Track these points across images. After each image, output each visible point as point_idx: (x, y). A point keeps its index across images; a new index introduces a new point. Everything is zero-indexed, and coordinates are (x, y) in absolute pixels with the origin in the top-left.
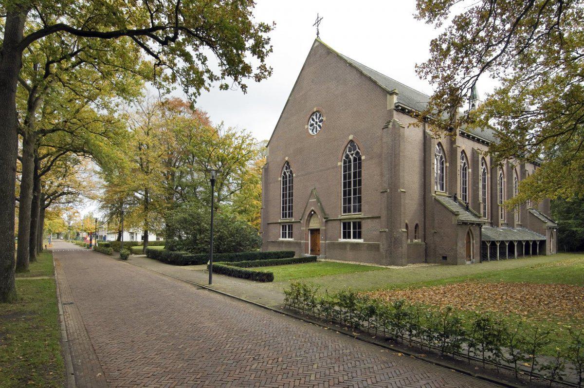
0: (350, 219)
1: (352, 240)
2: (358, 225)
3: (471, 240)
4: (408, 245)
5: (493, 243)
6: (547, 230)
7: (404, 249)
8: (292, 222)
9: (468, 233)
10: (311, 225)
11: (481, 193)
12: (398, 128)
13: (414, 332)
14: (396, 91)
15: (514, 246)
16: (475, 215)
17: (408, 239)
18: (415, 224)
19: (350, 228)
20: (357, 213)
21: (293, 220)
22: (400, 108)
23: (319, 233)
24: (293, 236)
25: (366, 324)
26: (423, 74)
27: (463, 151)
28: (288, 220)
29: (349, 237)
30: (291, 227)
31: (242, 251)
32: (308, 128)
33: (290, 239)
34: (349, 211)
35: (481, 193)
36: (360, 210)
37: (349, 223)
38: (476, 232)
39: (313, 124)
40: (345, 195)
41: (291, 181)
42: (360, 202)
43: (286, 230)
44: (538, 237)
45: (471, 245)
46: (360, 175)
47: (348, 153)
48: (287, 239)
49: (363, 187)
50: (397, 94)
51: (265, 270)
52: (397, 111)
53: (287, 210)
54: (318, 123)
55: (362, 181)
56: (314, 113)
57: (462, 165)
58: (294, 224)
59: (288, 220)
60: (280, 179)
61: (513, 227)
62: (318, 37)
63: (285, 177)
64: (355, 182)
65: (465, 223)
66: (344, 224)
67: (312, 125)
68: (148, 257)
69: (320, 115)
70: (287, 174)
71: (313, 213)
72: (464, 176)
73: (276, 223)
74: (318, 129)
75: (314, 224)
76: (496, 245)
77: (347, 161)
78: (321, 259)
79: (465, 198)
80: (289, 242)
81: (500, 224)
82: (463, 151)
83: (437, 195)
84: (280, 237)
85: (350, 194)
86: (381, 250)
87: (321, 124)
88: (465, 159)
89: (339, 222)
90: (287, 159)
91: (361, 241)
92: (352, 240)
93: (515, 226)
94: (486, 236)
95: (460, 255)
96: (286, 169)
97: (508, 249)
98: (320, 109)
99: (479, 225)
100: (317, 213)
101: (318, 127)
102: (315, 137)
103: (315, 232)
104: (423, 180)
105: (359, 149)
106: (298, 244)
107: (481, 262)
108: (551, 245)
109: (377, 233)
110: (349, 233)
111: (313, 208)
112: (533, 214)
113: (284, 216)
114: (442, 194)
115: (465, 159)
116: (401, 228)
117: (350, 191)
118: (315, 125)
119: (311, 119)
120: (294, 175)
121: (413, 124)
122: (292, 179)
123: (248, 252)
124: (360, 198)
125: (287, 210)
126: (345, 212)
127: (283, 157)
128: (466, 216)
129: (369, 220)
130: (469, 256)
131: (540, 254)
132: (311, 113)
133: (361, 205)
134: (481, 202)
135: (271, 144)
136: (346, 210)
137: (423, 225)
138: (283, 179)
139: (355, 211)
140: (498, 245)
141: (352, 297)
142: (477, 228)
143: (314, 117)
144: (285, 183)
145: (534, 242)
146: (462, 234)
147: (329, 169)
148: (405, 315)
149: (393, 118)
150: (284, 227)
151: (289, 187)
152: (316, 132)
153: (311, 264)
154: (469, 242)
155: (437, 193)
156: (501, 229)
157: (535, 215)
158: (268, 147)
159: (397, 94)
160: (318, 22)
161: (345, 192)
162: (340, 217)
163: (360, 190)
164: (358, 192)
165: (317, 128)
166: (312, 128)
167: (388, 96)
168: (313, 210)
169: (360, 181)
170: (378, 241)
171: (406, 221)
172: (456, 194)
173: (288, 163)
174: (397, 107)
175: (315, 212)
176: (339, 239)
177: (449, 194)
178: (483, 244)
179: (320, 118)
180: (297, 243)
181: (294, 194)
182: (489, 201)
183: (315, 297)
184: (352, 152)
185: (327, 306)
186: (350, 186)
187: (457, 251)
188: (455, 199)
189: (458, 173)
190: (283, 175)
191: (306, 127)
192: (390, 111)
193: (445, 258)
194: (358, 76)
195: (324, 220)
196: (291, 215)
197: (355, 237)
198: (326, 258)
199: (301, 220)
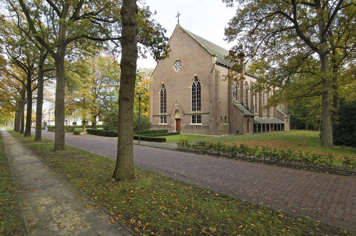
0: (196, 114)
1: (197, 124)
2: (199, 117)
3: (249, 124)
4: (222, 126)
5: (259, 125)
6: (285, 119)
7: (220, 128)
9: (248, 120)
11: (254, 102)
12: (217, 72)
13: (224, 151)
14: (216, 55)
15: (280, 125)
16: (251, 112)
17: (222, 123)
18: (225, 116)
19: (195, 118)
20: (199, 111)
21: (167, 114)
22: (218, 63)
23: (180, 121)
24: (201, 122)
25: (209, 151)
26: (227, 59)
27: (246, 82)
28: (164, 114)
29: (195, 123)
30: (165, 118)
31: (143, 130)
32: (174, 68)
33: (165, 124)
34: (195, 110)
35: (254, 102)
36: (200, 110)
37: (195, 116)
38: (251, 119)
39: (176, 66)
40: (193, 102)
41: (165, 94)
42: (200, 105)
43: (162, 119)
44: (280, 122)
45: (249, 126)
46: (200, 93)
47: (194, 82)
48: (163, 124)
49: (201, 99)
50: (216, 56)
51: (162, 137)
52: (217, 64)
53: (164, 108)
54: (179, 66)
55: (201, 96)
56: (177, 61)
57: (246, 88)
58: (167, 116)
59: (164, 114)
60: (160, 93)
61: (269, 118)
62: (178, 23)
63: (161, 92)
64: (197, 96)
65: (246, 116)
66: (193, 116)
67: (176, 67)
68: (88, 134)
69: (180, 62)
70: (163, 90)
71: (177, 111)
72: (247, 93)
73: (157, 116)
74: (179, 69)
75: (177, 116)
76: (261, 126)
77: (194, 85)
78: (181, 133)
79: (247, 104)
80: (165, 126)
81: (263, 116)
82: (246, 82)
83: (234, 103)
84: (191, 123)
85: (195, 102)
86: (210, 128)
87: (180, 67)
88: (247, 85)
90: (163, 83)
91: (201, 124)
92: (197, 124)
93: (270, 117)
94: (256, 121)
95: (244, 130)
96: (163, 88)
97: (266, 127)
99: (253, 117)
100: (179, 111)
101: (179, 68)
102: (178, 73)
103: (178, 120)
104: (228, 96)
106: (169, 126)
107: (253, 134)
108: (287, 126)
109: (208, 120)
110: (195, 120)
111: (177, 108)
112: (279, 111)
113: (162, 112)
114: (237, 102)
115: (247, 85)
116: (219, 118)
117: (195, 100)
118: (177, 67)
120: (167, 91)
121: (223, 80)
122: (166, 94)
123: (147, 130)
124: (200, 104)
125: (164, 108)
126: (193, 110)
127: (159, 82)
128: (247, 113)
129: (204, 115)
130: (248, 131)
131: (281, 130)
132: (175, 61)
133: (200, 107)
134: (255, 105)
135: (154, 75)
136: (194, 109)
137: (228, 116)
138: (161, 93)
139: (198, 110)
140: (262, 126)
141: (204, 143)
142: (252, 118)
143: (177, 63)
144: (162, 95)
145: (279, 124)
146: (245, 120)
148: (221, 146)
149: (215, 67)
150: (162, 118)
151: (164, 97)
152: (178, 70)
153: (177, 135)
154: (248, 125)
155: (234, 102)
156: (263, 118)
157: (280, 111)
159: (216, 56)
160: (178, 15)
161: (193, 101)
162: (190, 113)
163: (200, 100)
164: (199, 101)
165: (178, 69)
166: (176, 68)
167: (213, 57)
168: (177, 109)
169: (200, 96)
170: (209, 124)
171: (221, 115)
172: (243, 102)
173: (163, 85)
174: (217, 62)
175: (178, 110)
177: (240, 102)
178: (255, 125)
179: (180, 64)
180: (169, 126)
181: (167, 101)
182: (258, 105)
183: (190, 144)
184: (196, 82)
185: (195, 147)
186: (195, 98)
187: (243, 128)
188: (243, 104)
189: (244, 92)
190: (161, 91)
191: (173, 67)
192: (214, 64)
193: (238, 132)
194: (198, 46)
195: (183, 114)
196: (165, 111)
198: (184, 133)
199: (171, 114)
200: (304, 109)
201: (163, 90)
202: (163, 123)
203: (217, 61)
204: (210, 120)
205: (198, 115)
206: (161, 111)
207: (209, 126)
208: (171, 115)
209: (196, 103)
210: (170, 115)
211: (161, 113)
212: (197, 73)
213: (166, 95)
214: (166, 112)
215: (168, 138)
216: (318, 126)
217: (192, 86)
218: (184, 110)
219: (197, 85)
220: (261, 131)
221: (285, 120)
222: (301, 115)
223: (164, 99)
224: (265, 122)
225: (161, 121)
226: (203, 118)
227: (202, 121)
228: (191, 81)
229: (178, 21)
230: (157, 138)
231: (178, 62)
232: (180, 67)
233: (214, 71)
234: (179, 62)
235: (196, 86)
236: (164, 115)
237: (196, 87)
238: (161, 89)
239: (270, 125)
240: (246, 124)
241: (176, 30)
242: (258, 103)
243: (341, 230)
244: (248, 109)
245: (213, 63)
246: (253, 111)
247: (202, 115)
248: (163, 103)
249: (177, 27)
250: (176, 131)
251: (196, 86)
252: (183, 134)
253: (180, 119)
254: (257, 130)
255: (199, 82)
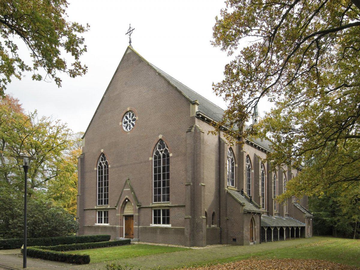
0: (160, 207)
1: (162, 225)
2: (167, 212)
5: (269, 228)
6: (306, 219)
8: (108, 209)
9: (252, 220)
10: (125, 211)
14: (197, 102)
15: (299, 229)
16: (256, 207)
18: (212, 213)
20: (166, 202)
21: (109, 207)
22: (201, 116)
23: (133, 219)
28: (104, 206)
29: (159, 223)
30: (106, 213)
36: (168, 200)
37: (159, 211)
38: (257, 219)
41: (107, 171)
42: (168, 192)
44: (300, 224)
47: (158, 149)
48: (103, 224)
50: (198, 104)
51: (82, 253)
52: (198, 118)
54: (131, 121)
56: (127, 112)
59: (104, 206)
63: (100, 167)
66: (155, 211)
67: (126, 123)
69: (133, 115)
71: (127, 200)
73: (92, 209)
74: (132, 126)
76: (271, 230)
77: (157, 157)
78: (135, 241)
80: (105, 227)
87: (134, 122)
89: (150, 209)
90: (102, 151)
91: (169, 226)
92: (162, 225)
96: (102, 160)
98: (133, 109)
100: (131, 201)
101: (129, 118)
105: (167, 147)
106: (113, 229)
107: (260, 243)
108: (308, 231)
111: (127, 197)
113: (100, 203)
114: (233, 188)
118: (128, 123)
119: (125, 118)
120: (109, 166)
122: (108, 170)
125: (103, 198)
129: (176, 208)
132: (125, 112)
136: (157, 199)
139: (164, 200)
143: (128, 116)
144: (100, 173)
147: (141, 162)
149: (195, 124)
150: (100, 214)
151: (105, 176)
152: (130, 129)
157: (298, 207)
158: (84, 139)
159: (198, 104)
160: (130, 31)
162: (151, 205)
163: (168, 182)
166: (126, 125)
167: (191, 105)
168: (127, 199)
169: (168, 175)
172: (243, 189)
175: (129, 200)
176: (151, 225)
178: (262, 229)
179: (133, 117)
181: (109, 183)
184: (162, 149)
186: (160, 179)
188: (242, 193)
189: (245, 172)
190: (98, 165)
191: (120, 123)
192: (193, 118)
193: (234, 240)
196: (106, 202)
197: (164, 223)
200: (332, 204)
201: (103, 163)
202: (102, 223)
203: (198, 113)
204: (185, 218)
205: (163, 208)
206: (99, 201)
207: (184, 229)
208: (117, 208)
209: (162, 194)
210: (115, 209)
211: (99, 204)
212: (163, 134)
213: (108, 173)
214: (108, 204)
215: (93, 253)
216: (353, 232)
217: (154, 157)
218: (140, 200)
219: (163, 154)
220: (271, 239)
221: (306, 221)
222: (329, 213)
223: (105, 179)
224: (277, 223)
225: (99, 219)
226: (173, 214)
227: (171, 220)
228: (151, 151)
229: (130, 42)
230: (71, 255)
231: (130, 114)
232: (132, 124)
233: (193, 130)
234: (131, 115)
235: (162, 157)
236: (104, 209)
237: (162, 159)
238: (99, 163)
239: (285, 229)
240: (248, 228)
241: (125, 58)
242: (265, 192)
243: (14, 124)
244: (250, 201)
245: (191, 116)
246: (259, 204)
247: (171, 209)
248: (103, 187)
249: (128, 52)
250: (125, 238)
251: (162, 157)
252: (136, 243)
253: (131, 216)
254: (271, 236)
255: (166, 149)
